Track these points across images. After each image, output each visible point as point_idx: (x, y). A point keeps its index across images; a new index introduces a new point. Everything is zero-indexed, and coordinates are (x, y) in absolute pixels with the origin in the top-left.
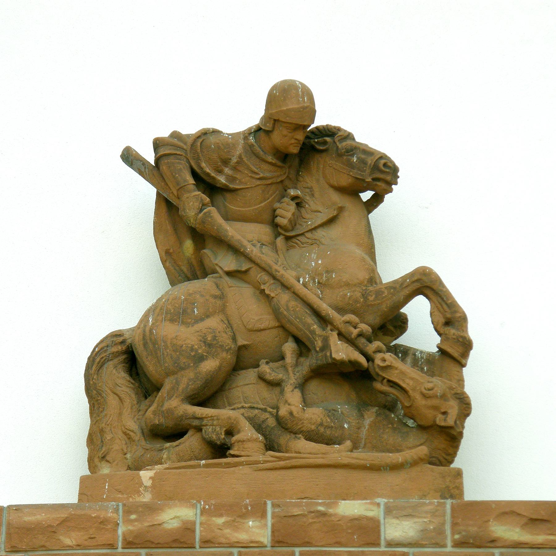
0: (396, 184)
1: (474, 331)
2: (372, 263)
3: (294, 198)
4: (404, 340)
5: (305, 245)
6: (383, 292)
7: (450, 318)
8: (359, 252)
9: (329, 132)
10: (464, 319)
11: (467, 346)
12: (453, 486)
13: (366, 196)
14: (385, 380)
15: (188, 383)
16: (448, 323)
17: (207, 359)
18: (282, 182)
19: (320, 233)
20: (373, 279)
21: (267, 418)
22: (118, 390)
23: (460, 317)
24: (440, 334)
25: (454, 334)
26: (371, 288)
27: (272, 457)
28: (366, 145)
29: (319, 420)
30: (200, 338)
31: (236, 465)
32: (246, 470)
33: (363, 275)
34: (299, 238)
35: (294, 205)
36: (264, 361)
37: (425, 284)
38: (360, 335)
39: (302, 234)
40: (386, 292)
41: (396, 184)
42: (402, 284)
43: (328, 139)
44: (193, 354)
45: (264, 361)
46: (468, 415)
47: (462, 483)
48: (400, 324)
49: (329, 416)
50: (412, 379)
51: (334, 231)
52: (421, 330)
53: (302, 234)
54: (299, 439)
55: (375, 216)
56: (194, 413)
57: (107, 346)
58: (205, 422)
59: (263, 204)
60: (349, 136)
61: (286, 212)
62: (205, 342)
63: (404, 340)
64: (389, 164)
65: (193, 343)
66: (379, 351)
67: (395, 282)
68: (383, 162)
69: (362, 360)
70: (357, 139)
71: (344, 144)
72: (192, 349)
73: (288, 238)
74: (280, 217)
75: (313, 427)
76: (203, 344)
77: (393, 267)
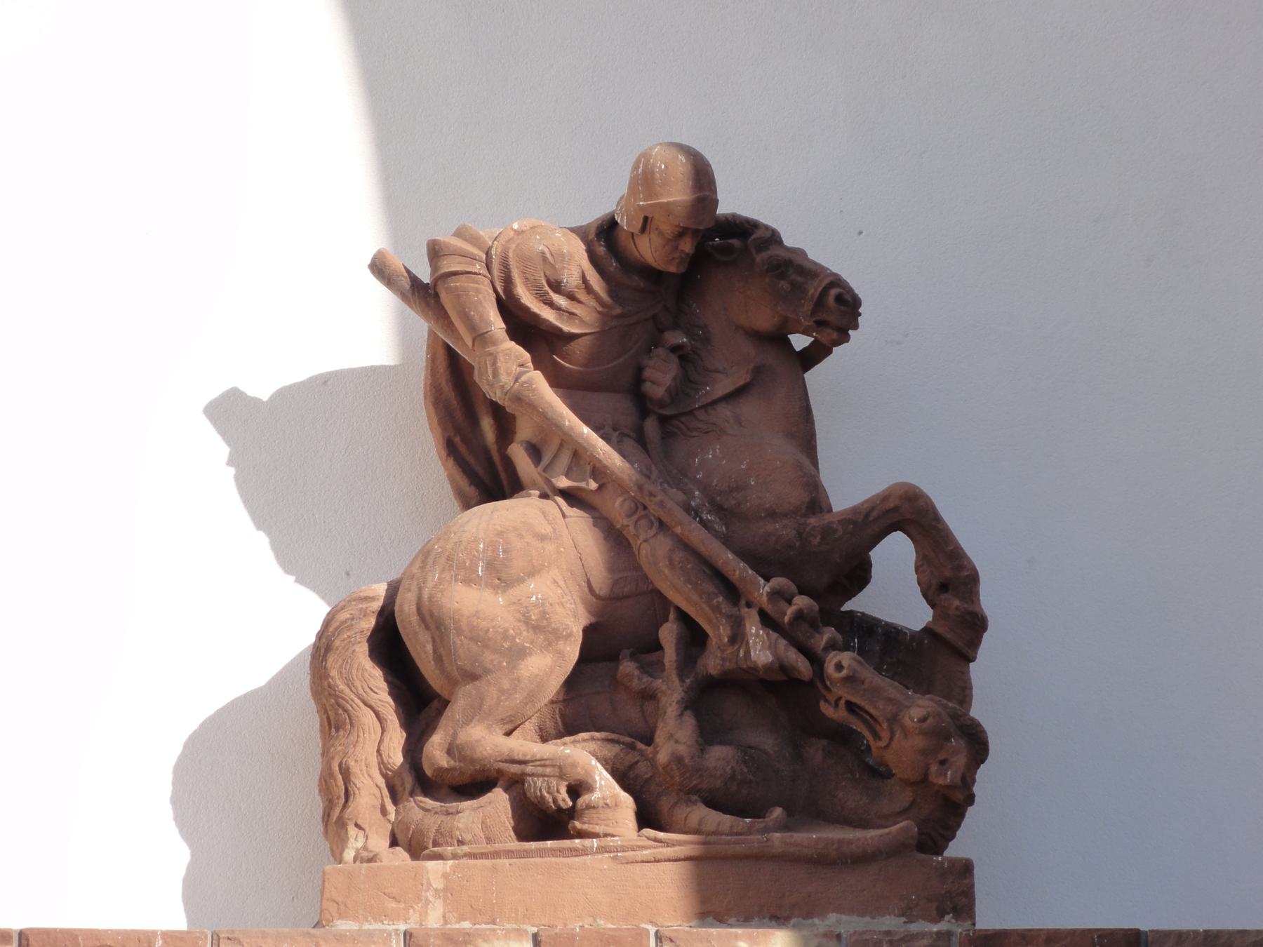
0: (856, 327)
1: (989, 599)
2: (811, 468)
3: (676, 349)
4: (861, 603)
5: (694, 434)
6: (836, 531)
7: (949, 576)
8: (788, 452)
9: (741, 229)
10: (974, 579)
11: (976, 625)
12: (956, 891)
13: (800, 342)
14: (842, 702)
15: (498, 698)
16: (944, 587)
17: (530, 654)
18: (654, 317)
19: (724, 411)
20: (816, 502)
21: (637, 762)
22: (372, 698)
23: (967, 576)
24: (932, 605)
25: (957, 608)
26: (813, 521)
27: (649, 839)
28: (802, 253)
29: (728, 769)
30: (518, 615)
31: (584, 852)
32: (604, 861)
33: (796, 496)
34: (683, 419)
35: (676, 360)
36: (627, 652)
37: (910, 513)
38: (799, 616)
39: (691, 413)
40: (840, 528)
41: (856, 327)
42: (867, 515)
43: (735, 242)
44: (506, 645)
45: (627, 652)
46: (983, 762)
47: (972, 886)
48: (859, 575)
49: (745, 762)
50: (890, 700)
51: (749, 409)
52: (894, 590)
53: (691, 413)
54: (694, 803)
55: (815, 378)
56: (511, 750)
57: (352, 619)
58: (529, 769)
59: (621, 360)
60: (774, 238)
61: (661, 376)
62: (527, 623)
63: (861, 603)
64: (848, 297)
65: (506, 625)
66: (832, 646)
67: (855, 510)
68: (834, 292)
69: (802, 666)
70: (788, 241)
71: (765, 255)
72: (505, 637)
73: (663, 420)
74: (652, 382)
75: (719, 783)
76: (523, 628)
77: (849, 484)
